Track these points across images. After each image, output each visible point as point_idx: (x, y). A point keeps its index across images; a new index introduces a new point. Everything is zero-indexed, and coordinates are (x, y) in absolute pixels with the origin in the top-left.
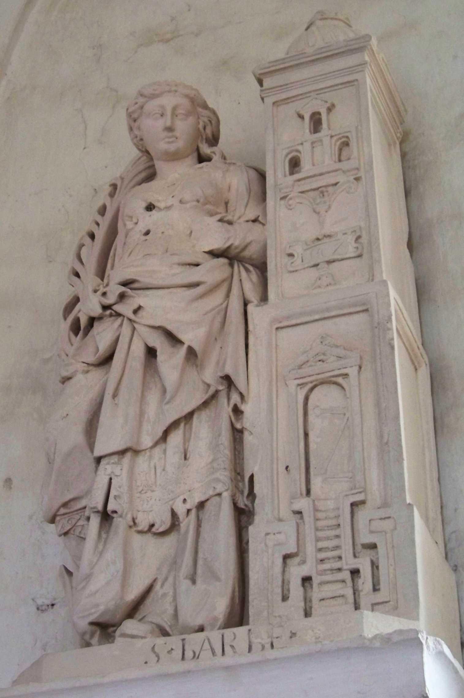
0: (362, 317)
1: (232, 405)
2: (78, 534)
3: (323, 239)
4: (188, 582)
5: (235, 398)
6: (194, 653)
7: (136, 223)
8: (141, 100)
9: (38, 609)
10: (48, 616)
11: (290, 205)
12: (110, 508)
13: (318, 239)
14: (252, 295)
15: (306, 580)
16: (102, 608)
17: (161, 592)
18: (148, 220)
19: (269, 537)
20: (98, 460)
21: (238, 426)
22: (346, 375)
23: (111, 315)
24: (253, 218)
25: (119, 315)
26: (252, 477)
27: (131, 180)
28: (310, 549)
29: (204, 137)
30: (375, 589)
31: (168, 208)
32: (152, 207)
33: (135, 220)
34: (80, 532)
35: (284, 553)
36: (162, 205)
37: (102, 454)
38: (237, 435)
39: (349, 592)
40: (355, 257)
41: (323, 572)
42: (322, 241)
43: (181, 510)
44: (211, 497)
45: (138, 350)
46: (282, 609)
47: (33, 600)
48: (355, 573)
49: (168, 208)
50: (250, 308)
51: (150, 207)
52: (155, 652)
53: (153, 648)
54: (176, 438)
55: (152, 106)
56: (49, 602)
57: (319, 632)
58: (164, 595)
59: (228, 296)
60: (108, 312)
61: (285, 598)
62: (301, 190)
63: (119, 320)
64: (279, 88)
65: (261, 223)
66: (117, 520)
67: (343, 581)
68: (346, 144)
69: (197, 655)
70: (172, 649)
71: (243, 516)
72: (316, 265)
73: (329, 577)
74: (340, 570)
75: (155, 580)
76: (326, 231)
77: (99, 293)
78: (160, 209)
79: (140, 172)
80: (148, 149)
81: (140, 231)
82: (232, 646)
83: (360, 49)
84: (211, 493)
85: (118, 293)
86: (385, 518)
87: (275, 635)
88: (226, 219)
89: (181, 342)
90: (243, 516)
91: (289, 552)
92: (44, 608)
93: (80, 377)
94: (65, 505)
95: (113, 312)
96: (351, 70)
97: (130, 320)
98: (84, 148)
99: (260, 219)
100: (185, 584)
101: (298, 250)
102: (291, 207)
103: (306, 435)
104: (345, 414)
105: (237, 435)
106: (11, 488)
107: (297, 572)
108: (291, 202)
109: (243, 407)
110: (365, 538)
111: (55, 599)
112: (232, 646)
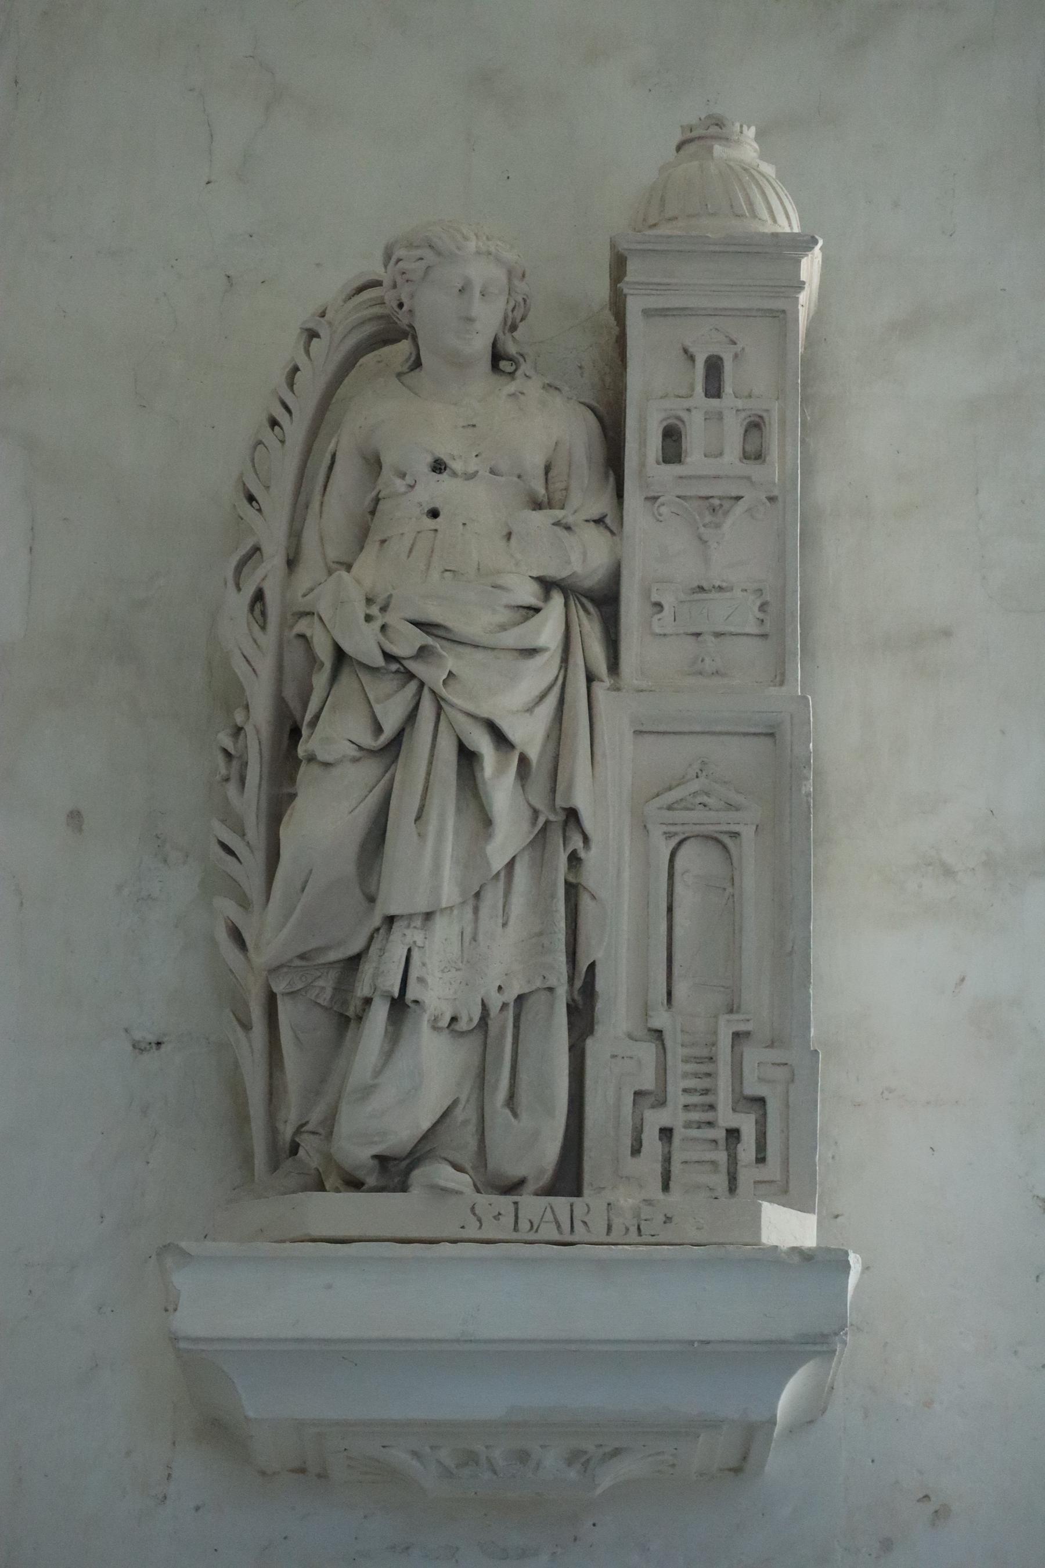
1: (569, 850)
2: (313, 998)
3: (710, 591)
5: (576, 842)
6: (531, 1223)
8: (430, 256)
9: (134, 1046)
11: (660, 515)
13: (701, 589)
14: (601, 667)
15: (666, 1133)
17: (460, 1118)
18: (435, 490)
22: (735, 835)
24: (596, 518)
25: (411, 676)
26: (592, 966)
28: (674, 1089)
29: (509, 323)
30: (761, 1159)
31: (470, 476)
33: (409, 480)
34: (317, 996)
35: (637, 1088)
36: (457, 466)
39: (722, 1156)
40: (756, 635)
41: (688, 1125)
42: (710, 596)
43: (495, 1002)
44: (538, 990)
46: (632, 1165)
47: (126, 1030)
48: (733, 1134)
49: (470, 476)
50: (596, 685)
51: (439, 467)
52: (474, 1214)
53: (473, 1209)
56: (152, 1038)
57: (702, 1221)
58: (465, 1123)
60: (394, 667)
61: (636, 1150)
62: (680, 494)
63: (413, 686)
64: (655, 287)
65: (607, 527)
67: (715, 1141)
69: (535, 1228)
70: (500, 1214)
72: (698, 635)
73: (694, 1133)
74: (710, 1124)
75: (455, 1103)
77: (376, 625)
78: (454, 474)
82: (585, 1223)
84: (538, 983)
86: (779, 1065)
87: (643, 1217)
89: (511, 746)
90: (582, 1015)
91: (644, 1088)
92: (143, 1046)
94: (302, 957)
95: (402, 669)
97: (433, 692)
98: (208, 183)
99: (608, 520)
102: (661, 518)
103: (670, 909)
104: (725, 889)
106: (80, 830)
107: (655, 1119)
108: (663, 509)
109: (582, 854)
110: (752, 1089)
111: (165, 1035)
112: (585, 1223)
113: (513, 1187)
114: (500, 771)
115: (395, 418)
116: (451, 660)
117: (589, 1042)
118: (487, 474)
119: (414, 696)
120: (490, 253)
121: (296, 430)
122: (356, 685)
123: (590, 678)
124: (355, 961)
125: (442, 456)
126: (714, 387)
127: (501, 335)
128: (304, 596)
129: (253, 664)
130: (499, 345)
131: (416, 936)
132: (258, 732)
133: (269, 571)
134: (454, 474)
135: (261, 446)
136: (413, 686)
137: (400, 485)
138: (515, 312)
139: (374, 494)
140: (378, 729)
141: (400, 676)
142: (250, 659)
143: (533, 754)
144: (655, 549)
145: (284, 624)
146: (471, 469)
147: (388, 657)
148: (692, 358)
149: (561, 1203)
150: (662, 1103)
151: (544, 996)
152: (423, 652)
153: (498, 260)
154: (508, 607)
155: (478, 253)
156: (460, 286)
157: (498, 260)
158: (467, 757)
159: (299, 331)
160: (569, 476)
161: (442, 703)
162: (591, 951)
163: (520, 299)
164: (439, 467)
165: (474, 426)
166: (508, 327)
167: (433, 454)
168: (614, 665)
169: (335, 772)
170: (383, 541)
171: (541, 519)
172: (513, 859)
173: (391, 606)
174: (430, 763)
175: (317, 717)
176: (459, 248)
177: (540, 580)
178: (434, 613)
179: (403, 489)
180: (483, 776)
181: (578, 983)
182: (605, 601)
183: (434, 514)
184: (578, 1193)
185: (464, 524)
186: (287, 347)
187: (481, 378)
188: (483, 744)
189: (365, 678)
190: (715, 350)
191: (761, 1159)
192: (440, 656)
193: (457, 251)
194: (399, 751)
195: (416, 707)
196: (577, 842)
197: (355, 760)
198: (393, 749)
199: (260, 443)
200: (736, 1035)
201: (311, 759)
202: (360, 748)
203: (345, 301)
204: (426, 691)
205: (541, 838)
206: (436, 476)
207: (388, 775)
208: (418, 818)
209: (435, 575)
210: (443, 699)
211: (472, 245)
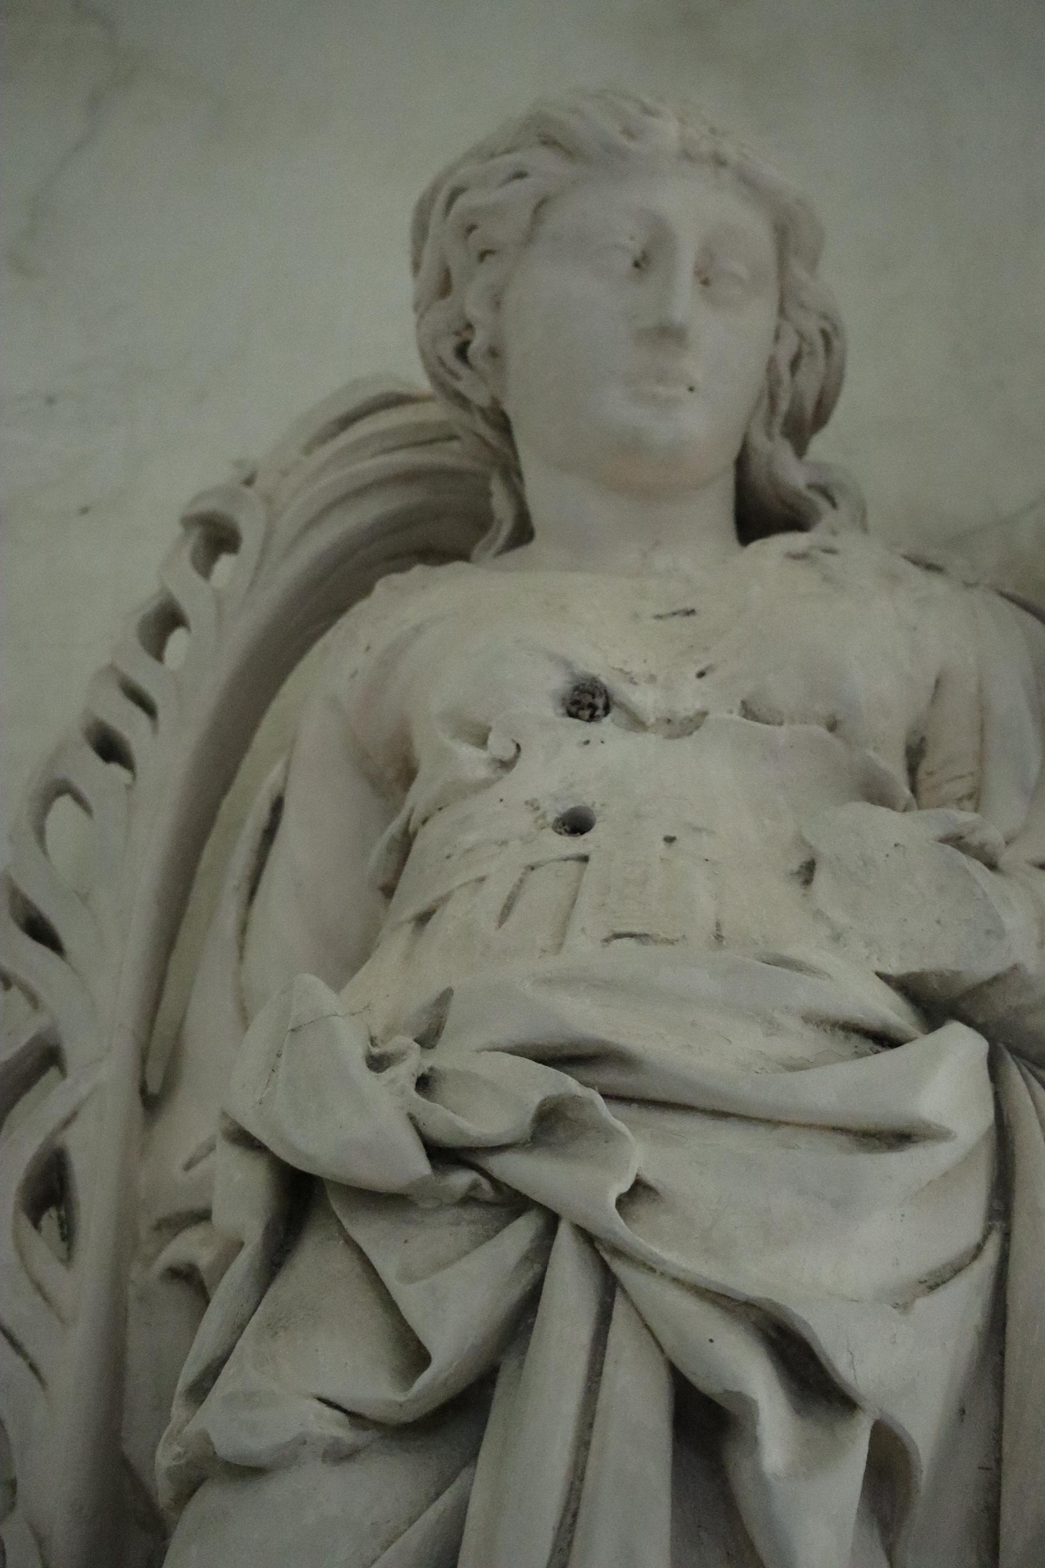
7: (506, 765)
8: (546, 164)
18: (570, 762)
23: (469, 1200)
25: (513, 1203)
27: (313, 523)
29: (784, 406)
31: (683, 727)
32: (600, 702)
33: (499, 746)
36: (645, 699)
49: (683, 727)
51: (587, 701)
60: (461, 1180)
63: (521, 1233)
77: (404, 1073)
78: (636, 723)
79: (360, 492)
80: (509, 408)
81: (533, 805)
85: (534, 1099)
88: (975, 840)
95: (485, 1184)
97: (587, 1238)
114: (812, 1461)
115: (458, 637)
116: (640, 1149)
118: (736, 717)
119: (526, 1259)
120: (720, 162)
121: (166, 754)
122: (341, 1261)
125: (594, 671)
127: (759, 439)
128: (188, 1166)
129: (29, 1348)
130: (757, 471)
132: (41, 1542)
134: (636, 723)
135: (65, 803)
137: (472, 761)
138: (802, 376)
139: (395, 827)
140: (414, 1356)
141: (475, 1213)
142: (20, 1336)
143: (923, 1427)
145: (124, 1251)
146: (688, 703)
147: (443, 1155)
152: (550, 1124)
153: (749, 183)
154: (810, 1019)
155: (687, 155)
156: (636, 248)
157: (749, 183)
158: (703, 1424)
159: (178, 530)
160: (981, 758)
161: (619, 1267)
163: (812, 326)
164: (587, 701)
165: (690, 612)
166: (779, 420)
167: (567, 664)
169: (275, 1491)
170: (423, 919)
173: (448, 1026)
174: (583, 1444)
175: (212, 1373)
176: (629, 133)
178: (587, 1019)
179: (482, 772)
180: (759, 1475)
183: (576, 824)
185: (670, 840)
186: (151, 560)
187: (699, 548)
188: (752, 1376)
189: (369, 1232)
192: (608, 1134)
193: (624, 141)
194: (481, 1439)
195: (530, 1303)
197: (339, 1455)
198: (457, 1419)
199: (62, 788)
202: (355, 1418)
203: (307, 450)
204: (564, 1235)
206: (580, 729)
207: (447, 1498)
209: (583, 946)
210: (618, 1252)
211: (668, 131)
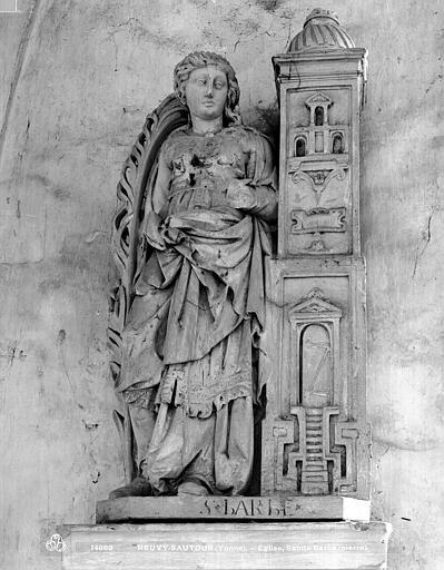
0: (344, 280)
4: (224, 456)
10: (95, 433)
12: (176, 402)
14: (268, 250)
16: (169, 470)
19: (277, 432)
20: (167, 366)
21: (255, 346)
28: (302, 444)
37: (172, 362)
38: (255, 352)
43: (219, 404)
45: (195, 288)
50: (267, 258)
54: (218, 353)
55: (199, 74)
59: (252, 246)
63: (180, 257)
66: (179, 410)
68: (339, 138)
71: (259, 411)
72: (313, 233)
76: (321, 205)
83: (356, 60)
90: (259, 411)
93: (149, 296)
94: (134, 385)
96: (348, 75)
100: (220, 458)
101: (300, 217)
105: (255, 352)
107: (293, 457)
113: (227, 492)
117: (263, 422)
123: (264, 254)
124: (156, 388)
126: (319, 121)
131: (178, 374)
133: (130, 218)
136: (180, 257)
144: (295, 194)
148: (309, 109)
149: (247, 500)
150: (297, 450)
151: (241, 401)
162: (267, 379)
168: (275, 251)
171: (241, 183)
172: (227, 337)
177: (240, 210)
181: (259, 394)
182: (271, 223)
184: (258, 494)
190: (319, 104)
191: (344, 474)
195: (180, 270)
196: (256, 327)
200: (331, 416)
201: (414, 370)
205: (239, 327)
208: (179, 320)
